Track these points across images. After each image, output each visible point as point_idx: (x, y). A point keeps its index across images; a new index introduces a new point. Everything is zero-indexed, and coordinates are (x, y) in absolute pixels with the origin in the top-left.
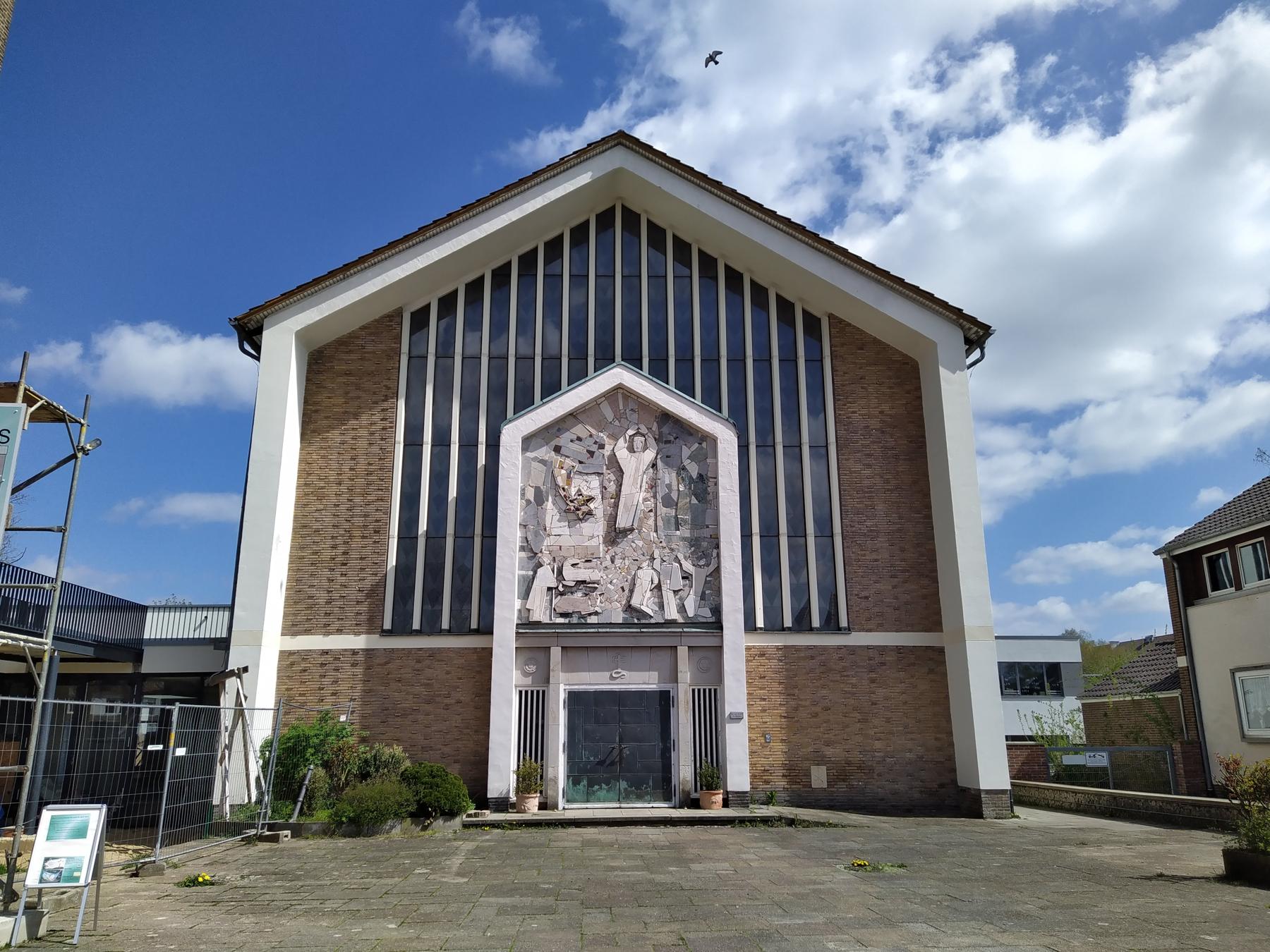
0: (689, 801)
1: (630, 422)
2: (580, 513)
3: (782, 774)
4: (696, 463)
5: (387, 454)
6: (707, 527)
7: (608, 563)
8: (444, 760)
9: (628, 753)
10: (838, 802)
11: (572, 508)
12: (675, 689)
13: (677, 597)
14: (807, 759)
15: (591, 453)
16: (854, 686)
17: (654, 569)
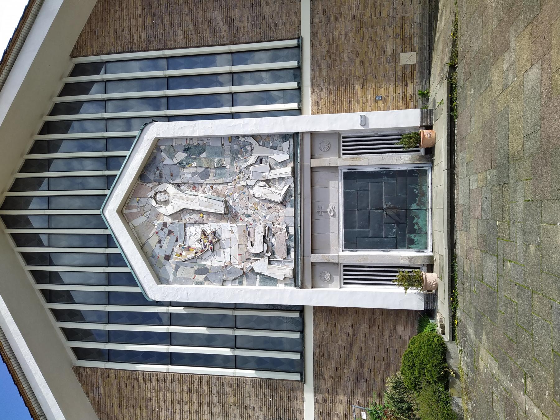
0: (428, 156)
1: (147, 203)
2: (214, 241)
3: (406, 87)
4: (175, 154)
5: (176, 378)
6: (223, 145)
7: (250, 219)
8: (394, 337)
9: (390, 203)
10: (427, 43)
11: (210, 246)
12: (343, 168)
13: (275, 168)
14: (395, 67)
15: (170, 232)
16: (340, 33)
17: (254, 185)
